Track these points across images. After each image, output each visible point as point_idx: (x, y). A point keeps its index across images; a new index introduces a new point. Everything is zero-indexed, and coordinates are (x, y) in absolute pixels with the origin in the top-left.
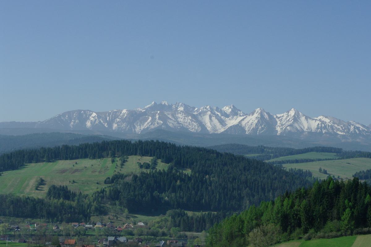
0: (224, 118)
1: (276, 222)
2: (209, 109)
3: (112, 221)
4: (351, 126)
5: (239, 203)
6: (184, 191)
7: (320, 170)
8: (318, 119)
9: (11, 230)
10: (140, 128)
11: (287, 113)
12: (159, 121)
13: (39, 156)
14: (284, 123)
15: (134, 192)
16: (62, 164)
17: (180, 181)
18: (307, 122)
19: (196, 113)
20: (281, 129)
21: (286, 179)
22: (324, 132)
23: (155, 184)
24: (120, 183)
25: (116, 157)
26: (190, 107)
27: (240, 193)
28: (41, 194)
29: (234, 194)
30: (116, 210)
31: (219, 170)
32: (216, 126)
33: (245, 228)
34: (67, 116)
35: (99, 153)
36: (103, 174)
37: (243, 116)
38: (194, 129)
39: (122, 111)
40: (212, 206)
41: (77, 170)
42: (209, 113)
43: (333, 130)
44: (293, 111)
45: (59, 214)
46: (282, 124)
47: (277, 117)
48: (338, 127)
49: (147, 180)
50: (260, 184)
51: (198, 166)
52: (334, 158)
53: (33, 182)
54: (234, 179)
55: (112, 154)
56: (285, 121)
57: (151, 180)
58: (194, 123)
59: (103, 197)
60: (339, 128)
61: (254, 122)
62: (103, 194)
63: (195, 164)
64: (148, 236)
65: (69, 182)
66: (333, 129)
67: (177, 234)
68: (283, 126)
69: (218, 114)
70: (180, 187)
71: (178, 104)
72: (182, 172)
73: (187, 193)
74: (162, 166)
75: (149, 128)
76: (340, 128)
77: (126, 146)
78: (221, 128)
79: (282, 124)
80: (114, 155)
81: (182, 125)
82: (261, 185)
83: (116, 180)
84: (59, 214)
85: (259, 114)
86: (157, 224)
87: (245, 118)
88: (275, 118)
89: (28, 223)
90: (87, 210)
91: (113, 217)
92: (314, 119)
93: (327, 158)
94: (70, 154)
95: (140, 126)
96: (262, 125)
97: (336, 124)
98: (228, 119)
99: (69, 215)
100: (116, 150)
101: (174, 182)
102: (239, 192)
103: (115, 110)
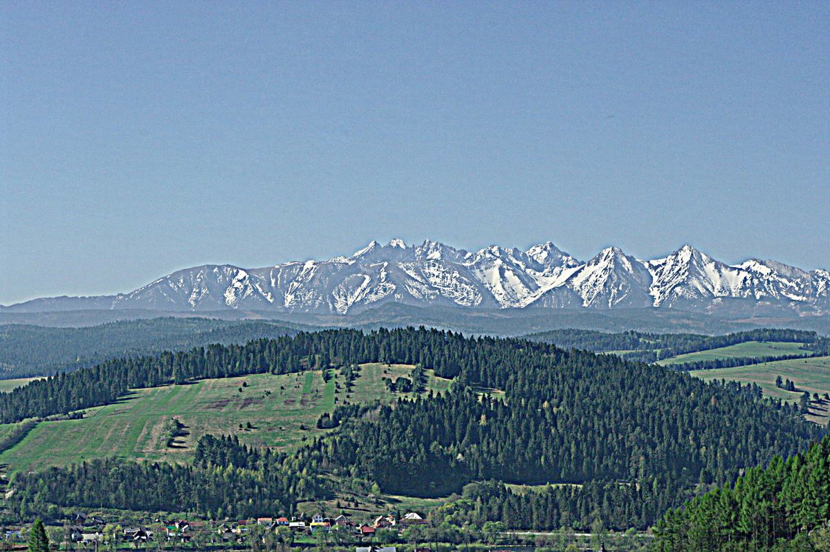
0: (532, 273)
1: (817, 503)
2: (498, 255)
3: (347, 511)
4: (818, 281)
5: (621, 462)
6: (497, 438)
7: (779, 381)
8: (744, 269)
9: (128, 537)
10: (345, 301)
11: (673, 257)
12: (387, 285)
13: (160, 372)
14: (669, 278)
15: (389, 445)
16: (212, 387)
17: (488, 418)
18: (720, 276)
19: (467, 264)
20: (661, 293)
21: (717, 405)
22: (758, 297)
23: (432, 427)
24: (354, 427)
25: (333, 367)
26: (455, 250)
27: (623, 439)
28: (182, 456)
29: (608, 442)
30: (352, 487)
31: (567, 388)
32: (516, 291)
33: (743, 519)
34: (182, 281)
35: (292, 360)
36: (312, 406)
37: (574, 266)
38: (465, 300)
39: (304, 265)
40: (563, 472)
41: (248, 401)
42: (499, 262)
43: (779, 293)
44: (688, 251)
45: (227, 500)
46: (663, 282)
47: (650, 265)
48: (791, 284)
49: (414, 417)
50: (664, 418)
51: (520, 382)
52: (803, 355)
53: (159, 431)
54: (606, 409)
55: (323, 362)
56: (671, 275)
57: (423, 417)
58: (465, 286)
59: (320, 460)
60: (792, 286)
61: (600, 279)
62: (320, 450)
63: (512, 377)
64: (439, 544)
65: (239, 428)
66: (779, 290)
67: (497, 537)
68: (667, 286)
69: (518, 265)
70: (487, 429)
71: (428, 245)
72: (489, 396)
73: (505, 442)
74: (438, 385)
75: (366, 300)
76: (794, 285)
77: (352, 341)
78: (526, 295)
79: (663, 282)
80: (326, 364)
81: (440, 291)
82: (668, 420)
83: (342, 419)
84: (227, 500)
85: (611, 261)
86: (449, 516)
87: (579, 271)
88: (647, 270)
89: (159, 521)
90: (288, 490)
91: (347, 503)
92: (735, 269)
93: (788, 355)
94: (229, 364)
95: (346, 297)
96: (619, 285)
97: (785, 277)
98: (542, 274)
99: (250, 501)
100: (331, 352)
101: (474, 419)
102: (620, 438)
103: (289, 264)
